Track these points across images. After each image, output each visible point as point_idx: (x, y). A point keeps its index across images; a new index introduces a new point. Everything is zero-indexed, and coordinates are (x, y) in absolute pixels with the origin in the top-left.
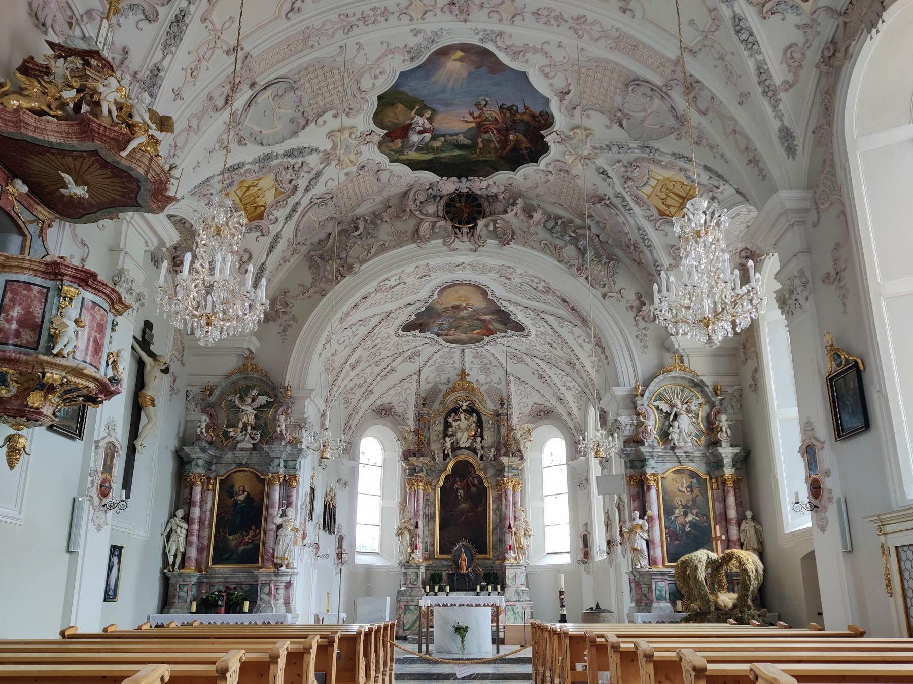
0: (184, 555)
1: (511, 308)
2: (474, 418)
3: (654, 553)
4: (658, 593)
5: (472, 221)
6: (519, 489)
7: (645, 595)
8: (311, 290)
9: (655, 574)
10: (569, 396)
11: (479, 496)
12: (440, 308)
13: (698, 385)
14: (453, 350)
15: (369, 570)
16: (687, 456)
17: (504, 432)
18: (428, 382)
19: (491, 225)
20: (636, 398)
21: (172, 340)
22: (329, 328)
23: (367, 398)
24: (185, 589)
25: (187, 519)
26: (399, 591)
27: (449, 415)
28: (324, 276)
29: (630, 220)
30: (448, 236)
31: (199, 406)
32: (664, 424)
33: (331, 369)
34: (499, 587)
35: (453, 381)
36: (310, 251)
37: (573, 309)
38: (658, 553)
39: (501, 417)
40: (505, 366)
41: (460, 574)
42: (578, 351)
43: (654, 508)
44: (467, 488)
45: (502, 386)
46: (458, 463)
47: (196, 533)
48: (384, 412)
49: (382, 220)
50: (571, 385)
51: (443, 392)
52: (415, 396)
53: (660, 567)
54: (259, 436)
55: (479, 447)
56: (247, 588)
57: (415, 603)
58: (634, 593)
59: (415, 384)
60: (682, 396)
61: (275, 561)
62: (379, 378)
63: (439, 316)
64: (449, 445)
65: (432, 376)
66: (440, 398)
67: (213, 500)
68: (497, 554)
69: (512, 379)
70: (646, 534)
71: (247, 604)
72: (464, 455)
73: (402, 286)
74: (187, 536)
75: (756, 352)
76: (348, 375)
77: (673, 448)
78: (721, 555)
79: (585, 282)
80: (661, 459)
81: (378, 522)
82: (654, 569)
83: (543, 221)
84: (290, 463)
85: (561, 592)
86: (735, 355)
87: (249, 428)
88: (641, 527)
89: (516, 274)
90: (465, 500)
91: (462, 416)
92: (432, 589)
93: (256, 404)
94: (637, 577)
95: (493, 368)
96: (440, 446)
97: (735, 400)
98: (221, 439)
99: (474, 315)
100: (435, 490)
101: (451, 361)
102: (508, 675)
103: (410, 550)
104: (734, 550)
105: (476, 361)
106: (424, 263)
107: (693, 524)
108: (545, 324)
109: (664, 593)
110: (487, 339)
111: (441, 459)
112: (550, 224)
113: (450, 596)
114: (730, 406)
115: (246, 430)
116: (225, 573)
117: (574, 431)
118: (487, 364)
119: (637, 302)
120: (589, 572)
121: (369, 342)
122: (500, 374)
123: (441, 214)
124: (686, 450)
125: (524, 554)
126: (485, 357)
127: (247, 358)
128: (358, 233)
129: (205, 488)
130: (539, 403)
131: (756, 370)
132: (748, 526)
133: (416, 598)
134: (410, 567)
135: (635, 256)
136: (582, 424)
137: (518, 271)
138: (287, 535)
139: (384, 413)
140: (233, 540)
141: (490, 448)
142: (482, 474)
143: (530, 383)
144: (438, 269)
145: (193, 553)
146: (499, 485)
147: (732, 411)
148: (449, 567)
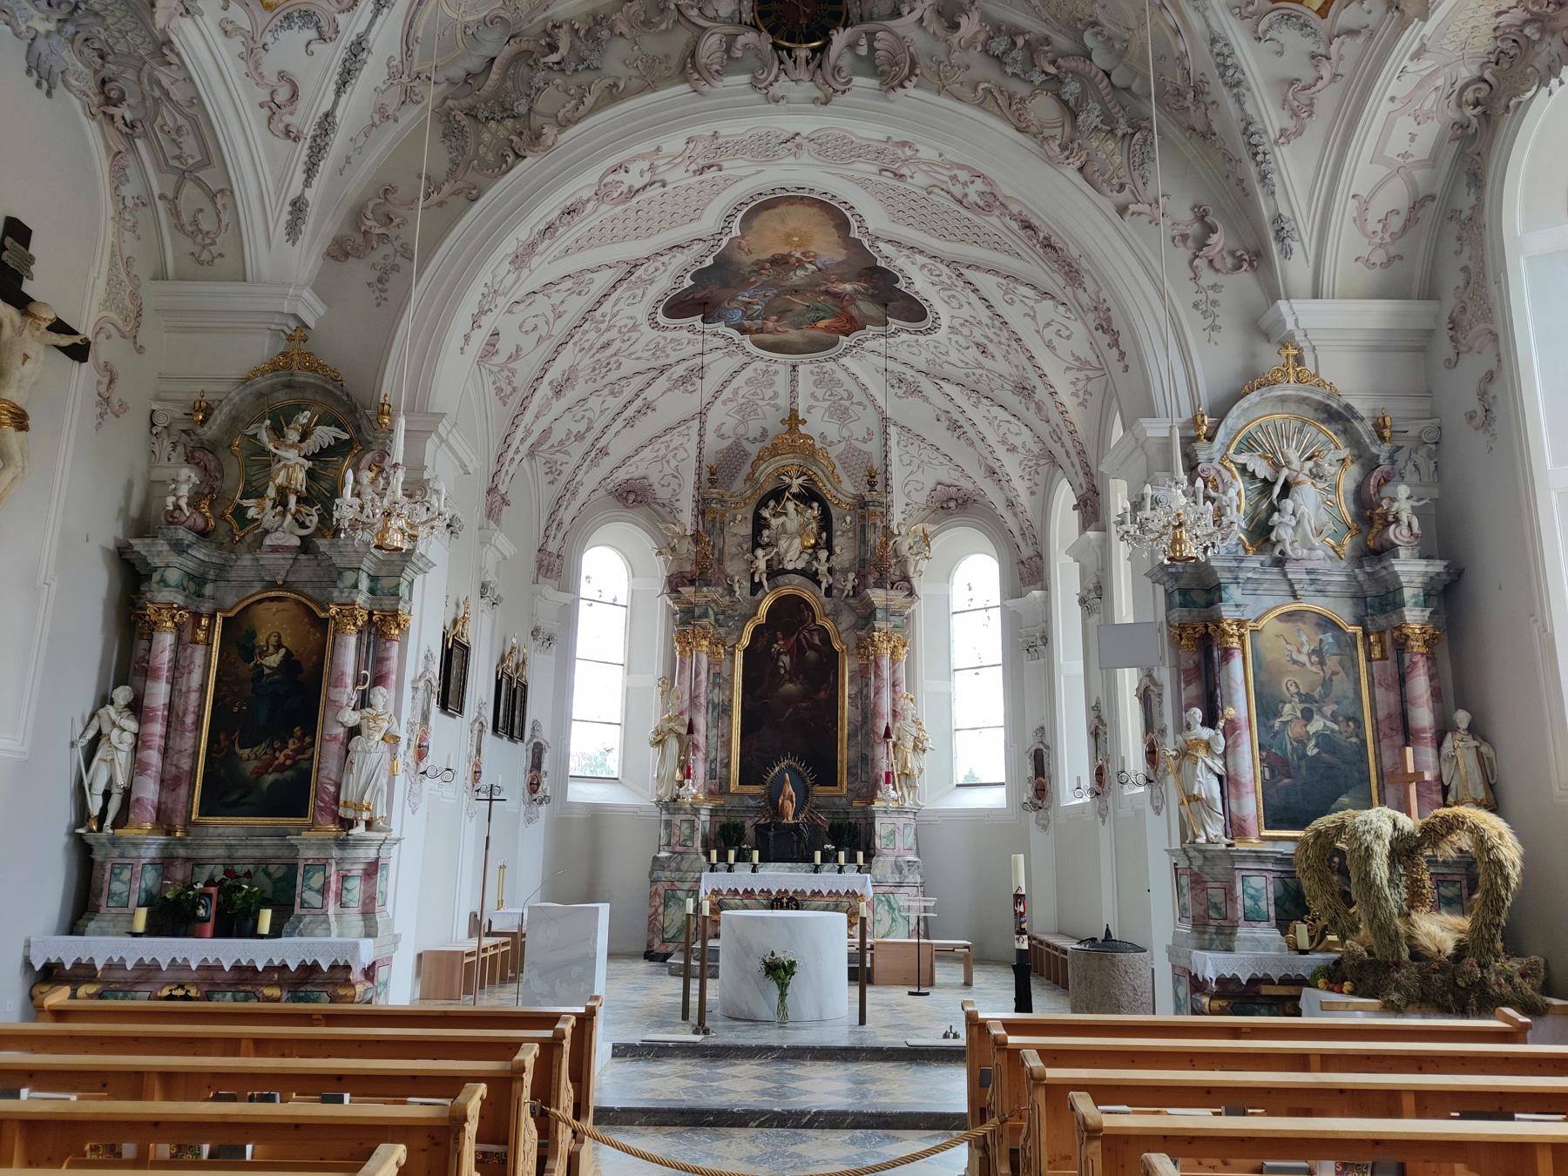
0: (127, 792)
1: (900, 262)
3: (1240, 807)
4: (1249, 902)
5: (819, 32)
6: (903, 654)
7: (1216, 907)
8: (446, 188)
9: (1244, 859)
10: (1011, 466)
11: (821, 669)
12: (746, 260)
13: (1337, 417)
14: (774, 367)
15: (596, 816)
16: (1313, 581)
17: (874, 538)
18: (722, 437)
19: (863, 41)
20: (1197, 445)
21: (102, 283)
22: (484, 277)
23: (595, 463)
24: (126, 874)
25: (137, 708)
26: (655, 859)
27: (763, 503)
28: (476, 155)
29: (1194, 19)
30: (765, 66)
31: (180, 448)
32: (1257, 506)
33: (509, 389)
34: (860, 855)
35: (771, 434)
36: (446, 99)
37: (1048, 244)
38: (1250, 806)
39: (868, 509)
40: (881, 402)
41: (779, 826)
42: (1044, 358)
43: (1240, 705)
44: (797, 652)
45: (873, 447)
46: (779, 602)
47: (158, 741)
48: (632, 497)
49: (611, 30)
50: (1017, 441)
51: (753, 457)
52: (694, 465)
53: (1253, 843)
54: (315, 519)
55: (823, 568)
56: (279, 874)
57: (686, 886)
58: (1188, 899)
59: (695, 438)
60: (1299, 443)
61: (341, 812)
62: (620, 423)
63: (745, 282)
65: (731, 423)
66: (747, 469)
67: (204, 667)
69: (892, 430)
70: (1220, 763)
71: (266, 916)
72: (794, 586)
73: (655, 191)
74: (135, 749)
75: (1495, 337)
76: (547, 405)
77: (1280, 562)
78: (1420, 823)
79: (1077, 178)
80: (1253, 586)
82: (1240, 846)
83: (982, 37)
84: (385, 583)
85: (1018, 898)
86: (1423, 349)
87: (293, 499)
88: (1208, 746)
89: (919, 161)
90: (793, 675)
91: (791, 506)
92: (723, 857)
93: (312, 445)
94: (1198, 863)
97: (1423, 451)
98: (225, 526)
99: (818, 285)
100: (733, 654)
101: (769, 393)
102: (893, 1116)
103: (678, 776)
104: (1461, 810)
105: (820, 392)
106: (703, 130)
107: (1324, 739)
108: (973, 298)
109: (1263, 904)
110: (844, 341)
111: (747, 592)
112: (999, 46)
113: (761, 872)
114: (1410, 464)
115: (285, 505)
116: (231, 837)
117: (1019, 539)
118: (850, 394)
119: (1196, 225)
120: (1045, 827)
121: (592, 335)
122: (870, 419)
123: (747, 17)
124: (1310, 565)
125: (912, 787)
126: (839, 383)
127: (290, 338)
128: (555, 57)
129: (187, 636)
130: (948, 481)
131: (1490, 377)
132: (1460, 747)
134: (678, 810)
135: (1196, 118)
136: (1037, 524)
137: (926, 153)
138: (371, 751)
139: (632, 497)
140: (249, 758)
141: (845, 571)
143: (930, 440)
144: (739, 148)
145: (149, 790)
146: (864, 646)
147: (1416, 478)
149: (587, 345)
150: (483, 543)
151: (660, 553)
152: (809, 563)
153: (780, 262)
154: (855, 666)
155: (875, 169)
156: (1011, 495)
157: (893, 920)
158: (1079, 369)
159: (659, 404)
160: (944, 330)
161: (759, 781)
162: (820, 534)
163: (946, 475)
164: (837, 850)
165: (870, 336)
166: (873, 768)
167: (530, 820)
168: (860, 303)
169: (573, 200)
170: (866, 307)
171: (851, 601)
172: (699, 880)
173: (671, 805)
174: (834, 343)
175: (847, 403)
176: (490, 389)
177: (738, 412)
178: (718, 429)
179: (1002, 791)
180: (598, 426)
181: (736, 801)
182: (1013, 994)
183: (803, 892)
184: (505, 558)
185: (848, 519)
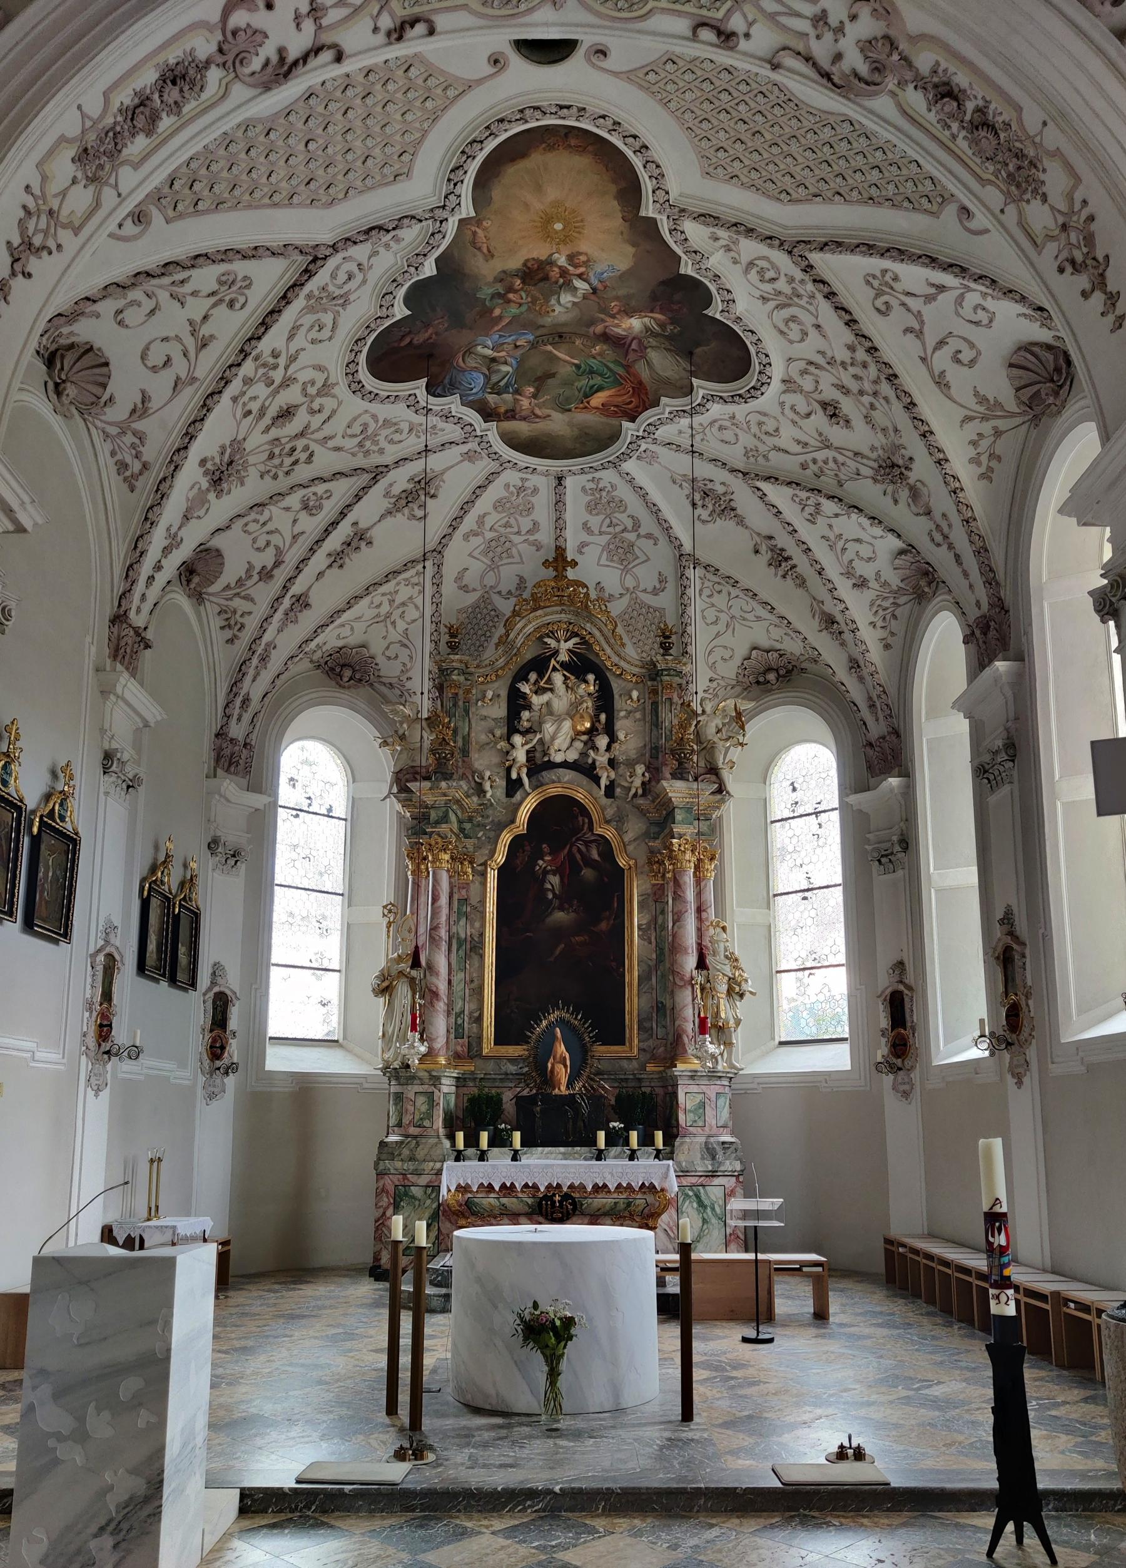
2: (591, 685)
10: (859, 608)
14: (535, 480)
15: (305, 1091)
17: (669, 718)
18: (465, 588)
23: (290, 617)
26: (383, 1144)
27: (521, 675)
33: (137, 466)
34: (659, 1136)
40: (682, 532)
42: (930, 405)
44: (569, 870)
45: (666, 601)
48: (346, 672)
55: (602, 759)
57: (423, 1180)
62: (320, 560)
63: (485, 319)
64: (520, 755)
65: (477, 566)
68: (651, 1043)
85: (995, 1220)
90: (563, 901)
91: (558, 678)
92: (472, 1141)
95: (645, 544)
96: (496, 760)
100: (484, 874)
101: (526, 523)
105: (595, 521)
110: (629, 429)
111: (501, 792)
113: (525, 1160)
121: (260, 390)
122: (660, 558)
126: (621, 505)
130: (765, 643)
136: (892, 691)
139: (347, 673)
141: (631, 764)
142: (609, 833)
143: (745, 582)
146: (660, 860)
148: (521, 1078)
149: (255, 406)
150: (105, 692)
151: (385, 743)
152: (584, 754)
153: (536, 275)
155: (682, 26)
156: (856, 652)
157: (705, 1221)
158: (984, 418)
159: (375, 533)
160: (776, 386)
161: (518, 1039)
163: (763, 633)
164: (627, 1129)
165: (669, 423)
167: (212, 1096)
168: (654, 355)
170: (661, 363)
171: (641, 801)
172: (439, 1173)
173: (399, 1073)
174: (614, 437)
175: (631, 537)
176: (107, 464)
177: (485, 553)
178: (459, 578)
179: (845, 1048)
180: (291, 558)
181: (490, 1066)
183: (582, 1187)
184: (146, 725)
185: (635, 694)
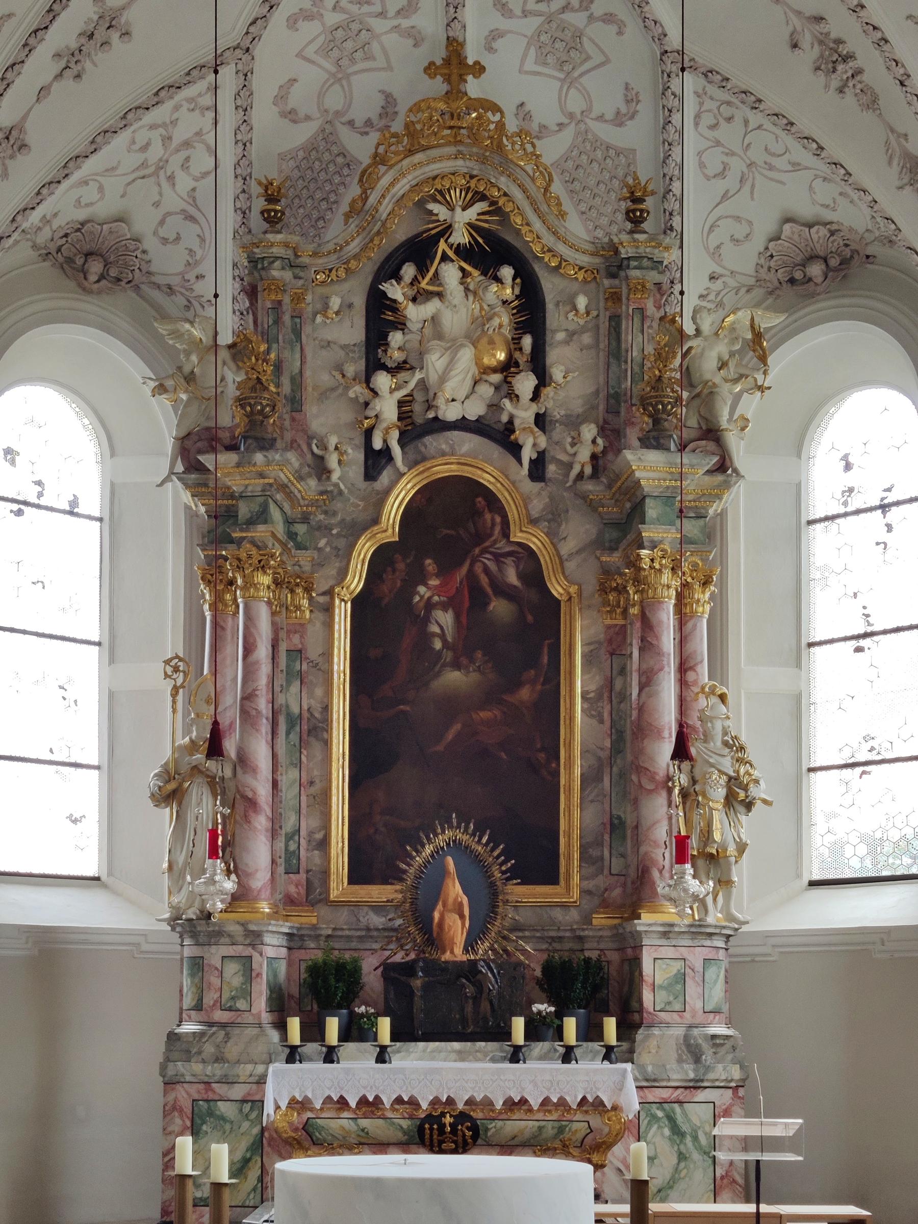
17: (639, 343)
18: (291, 115)
26: (173, 1037)
27: (389, 269)
34: (610, 1025)
41: (436, 969)
44: (471, 601)
45: (636, 136)
46: (430, 494)
55: (525, 414)
57: (238, 1092)
64: (387, 409)
72: (463, 457)
81: (90, 750)
95: (602, 33)
96: (347, 415)
100: (328, 609)
130: (806, 211)
133: (245, 1070)
139: (95, 267)
141: (574, 423)
142: (536, 540)
143: (773, 102)
146: (620, 588)
148: (393, 935)
151: (161, 389)
152: (495, 407)
154: (598, 631)
157: (682, 1157)
162: (517, 340)
163: (803, 193)
164: (560, 1015)
166: (637, 844)
169: (140, 101)
171: (589, 486)
172: (261, 1081)
177: (325, 51)
178: (281, 98)
181: (343, 917)
182: (413, 1044)
183: (488, 1103)
185: (582, 302)
